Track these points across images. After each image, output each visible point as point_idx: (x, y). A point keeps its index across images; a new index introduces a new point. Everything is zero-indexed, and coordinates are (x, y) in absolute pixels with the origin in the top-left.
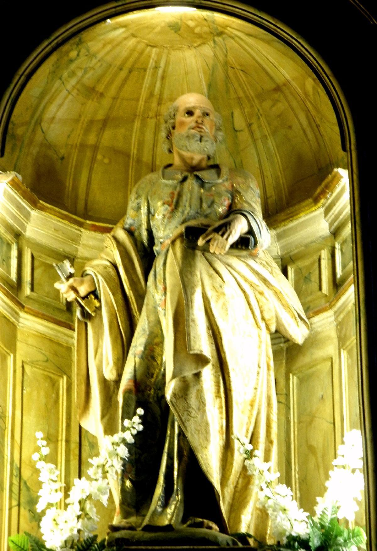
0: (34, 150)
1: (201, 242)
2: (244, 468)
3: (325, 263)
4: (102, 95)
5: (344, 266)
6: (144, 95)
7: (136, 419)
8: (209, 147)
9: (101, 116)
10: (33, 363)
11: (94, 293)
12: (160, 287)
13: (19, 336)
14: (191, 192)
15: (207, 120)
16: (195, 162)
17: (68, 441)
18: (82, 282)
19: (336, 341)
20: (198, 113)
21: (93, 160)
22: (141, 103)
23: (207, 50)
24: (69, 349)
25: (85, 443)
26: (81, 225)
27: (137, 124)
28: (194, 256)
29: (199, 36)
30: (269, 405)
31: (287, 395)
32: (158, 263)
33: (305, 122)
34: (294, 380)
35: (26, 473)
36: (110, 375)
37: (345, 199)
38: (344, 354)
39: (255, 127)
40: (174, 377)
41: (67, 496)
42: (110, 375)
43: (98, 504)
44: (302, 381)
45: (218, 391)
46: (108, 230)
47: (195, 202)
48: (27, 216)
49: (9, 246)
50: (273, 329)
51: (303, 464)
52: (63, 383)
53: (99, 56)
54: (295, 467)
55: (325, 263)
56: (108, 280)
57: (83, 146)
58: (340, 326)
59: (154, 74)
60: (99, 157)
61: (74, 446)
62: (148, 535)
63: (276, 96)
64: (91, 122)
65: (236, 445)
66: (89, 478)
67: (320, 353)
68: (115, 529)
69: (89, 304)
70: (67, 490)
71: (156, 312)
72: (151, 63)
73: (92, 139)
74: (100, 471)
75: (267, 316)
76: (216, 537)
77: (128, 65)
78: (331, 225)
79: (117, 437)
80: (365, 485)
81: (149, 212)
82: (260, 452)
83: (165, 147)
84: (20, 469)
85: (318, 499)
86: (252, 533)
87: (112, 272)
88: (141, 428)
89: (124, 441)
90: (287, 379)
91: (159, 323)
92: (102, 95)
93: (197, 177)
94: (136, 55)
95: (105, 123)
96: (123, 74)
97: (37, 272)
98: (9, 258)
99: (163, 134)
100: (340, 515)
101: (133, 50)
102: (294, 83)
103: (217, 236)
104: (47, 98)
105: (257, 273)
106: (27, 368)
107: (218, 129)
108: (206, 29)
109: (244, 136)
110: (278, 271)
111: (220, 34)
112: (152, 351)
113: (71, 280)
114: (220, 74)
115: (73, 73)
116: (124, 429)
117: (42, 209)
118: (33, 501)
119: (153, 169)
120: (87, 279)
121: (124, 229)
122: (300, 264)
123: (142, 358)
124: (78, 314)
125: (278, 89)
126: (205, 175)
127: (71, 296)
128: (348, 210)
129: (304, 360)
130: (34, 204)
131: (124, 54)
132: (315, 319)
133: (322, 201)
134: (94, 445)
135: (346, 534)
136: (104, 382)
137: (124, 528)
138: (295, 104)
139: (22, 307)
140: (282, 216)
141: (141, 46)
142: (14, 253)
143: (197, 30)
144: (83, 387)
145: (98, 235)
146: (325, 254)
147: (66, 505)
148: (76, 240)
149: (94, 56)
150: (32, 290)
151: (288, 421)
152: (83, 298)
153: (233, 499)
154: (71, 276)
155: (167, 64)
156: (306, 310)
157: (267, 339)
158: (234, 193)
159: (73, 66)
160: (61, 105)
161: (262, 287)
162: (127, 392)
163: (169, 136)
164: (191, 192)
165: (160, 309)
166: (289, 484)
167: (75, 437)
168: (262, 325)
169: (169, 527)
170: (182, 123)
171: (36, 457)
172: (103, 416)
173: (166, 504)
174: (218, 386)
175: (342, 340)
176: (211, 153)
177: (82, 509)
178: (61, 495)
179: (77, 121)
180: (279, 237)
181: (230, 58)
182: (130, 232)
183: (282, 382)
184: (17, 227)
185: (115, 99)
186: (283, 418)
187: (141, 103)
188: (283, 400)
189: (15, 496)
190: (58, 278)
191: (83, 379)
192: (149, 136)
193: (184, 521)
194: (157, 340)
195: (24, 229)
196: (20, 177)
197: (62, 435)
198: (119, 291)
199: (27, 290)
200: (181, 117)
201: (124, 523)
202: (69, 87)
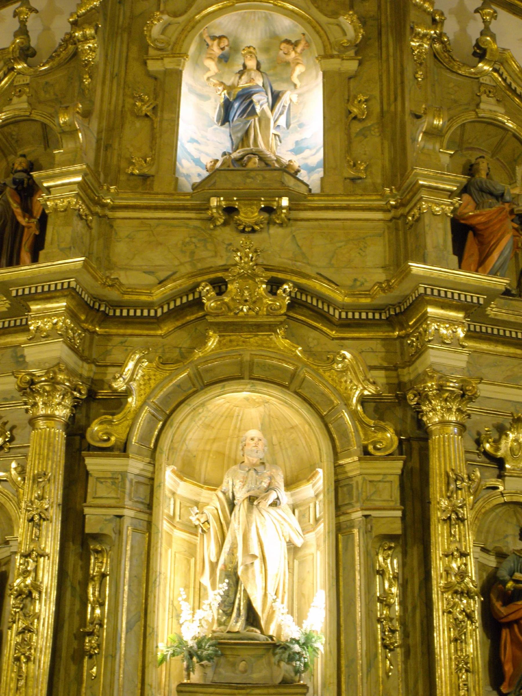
0: (182, 453)
1: (255, 503)
2: (272, 607)
3: (312, 510)
4: (213, 428)
5: (320, 513)
6: (232, 428)
7: (225, 584)
8: (261, 455)
9: (212, 437)
10: (180, 553)
11: (207, 521)
12: (237, 521)
13: (174, 540)
14: (252, 477)
15: (260, 442)
16: (254, 462)
17: (194, 588)
18: (202, 517)
19: (315, 546)
20: (256, 440)
21: (209, 456)
22: (231, 431)
23: (261, 409)
24: (195, 545)
25: (202, 590)
26: (202, 487)
27: (229, 441)
28: (252, 508)
29: (258, 403)
30: (285, 575)
31: (293, 569)
32: (236, 509)
33: (305, 444)
34: (296, 562)
35: (175, 603)
36: (214, 560)
37: (321, 482)
38: (319, 552)
39: (282, 444)
40: (242, 564)
41: (193, 617)
42: (214, 560)
43: (207, 621)
44: (300, 563)
45: (262, 571)
46: (215, 490)
47: (254, 482)
48: (178, 485)
49: (170, 499)
50: (288, 540)
51: (299, 601)
52: (192, 561)
53: (212, 411)
54: (295, 603)
55: (312, 510)
56: (214, 515)
57: (204, 451)
58: (318, 539)
59: (237, 419)
60: (211, 455)
61: (197, 590)
62: (229, 635)
63: (292, 430)
64: (208, 440)
65: (269, 596)
66: (203, 609)
67: (308, 551)
68: (214, 632)
69: (205, 526)
70: (193, 614)
71: (235, 533)
72: (236, 414)
73: (208, 447)
74: (208, 606)
75: (285, 534)
76: (259, 637)
77: (226, 414)
78: (315, 492)
79: (216, 592)
80: (326, 617)
81: (233, 484)
82: (279, 600)
83: (241, 453)
84: (172, 601)
85: (304, 621)
86: (275, 635)
87: (216, 511)
88: (227, 588)
89: (219, 594)
90: (293, 562)
91: (236, 537)
92: (213, 428)
93: (255, 470)
94: (229, 410)
95: (214, 440)
96: (223, 418)
97: (182, 510)
98: (170, 504)
99: (240, 448)
100: (313, 629)
101: (228, 408)
102: (300, 426)
103: (263, 501)
104: (189, 429)
105: (280, 515)
106: (177, 555)
107: (266, 446)
108: (261, 400)
109: (277, 448)
110: (291, 512)
111: (267, 402)
112: (233, 551)
113: (197, 516)
114: (267, 419)
115: (200, 419)
116: (220, 588)
117: (185, 481)
118: (178, 616)
119: (235, 463)
120: (204, 515)
121: (222, 492)
122: (301, 508)
123: (228, 554)
124: (200, 530)
125: (292, 428)
126: (259, 469)
127: (197, 523)
128: (322, 487)
129: (300, 554)
130: (181, 479)
131: (224, 410)
132: (307, 535)
133: (311, 481)
134: (206, 594)
135: (316, 638)
136: (211, 563)
137: (218, 632)
138: (300, 435)
139: (175, 527)
140: (293, 486)
141: (231, 407)
142: (172, 502)
143: (257, 400)
144: (202, 564)
145: (210, 492)
146: (312, 505)
147: (193, 621)
148: (199, 495)
149: (210, 411)
150: (180, 519)
151: (293, 581)
152: (203, 523)
153: (267, 618)
154: (197, 514)
155: (243, 414)
156: (303, 531)
157: (285, 544)
158: (271, 477)
159: (200, 416)
160: (194, 433)
161: (283, 522)
162: (221, 570)
163: (243, 449)
164: (252, 477)
165: (237, 531)
166: (292, 615)
167: (197, 586)
168: (283, 539)
169: (238, 632)
170: (249, 444)
171: (180, 599)
172: (210, 578)
173: (237, 622)
174: (262, 568)
175: (318, 546)
176: (261, 457)
177: (200, 623)
178: (191, 616)
179: (202, 439)
180: (292, 495)
181: (272, 413)
182: (224, 493)
183: (291, 563)
184: (173, 490)
185: (219, 429)
186: (291, 580)
187: (231, 431)
188: (291, 571)
189: (171, 614)
190: (191, 515)
191: (202, 561)
192: (234, 446)
193: (245, 628)
194: (235, 546)
195: (176, 490)
196: (175, 468)
197: (192, 585)
198: (219, 521)
199: (177, 519)
200: (248, 441)
201: (218, 629)
202: (198, 425)
